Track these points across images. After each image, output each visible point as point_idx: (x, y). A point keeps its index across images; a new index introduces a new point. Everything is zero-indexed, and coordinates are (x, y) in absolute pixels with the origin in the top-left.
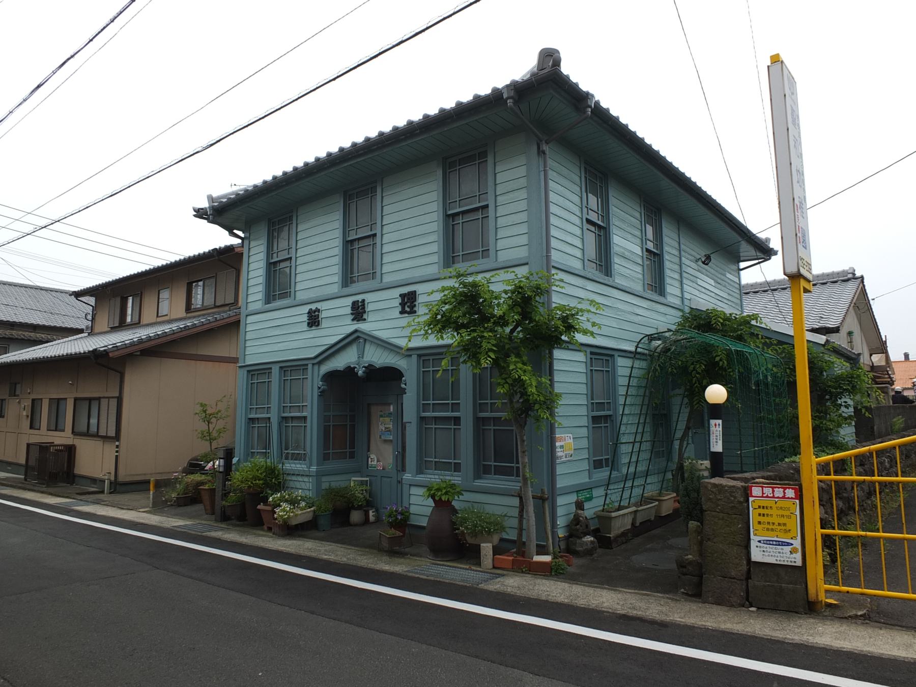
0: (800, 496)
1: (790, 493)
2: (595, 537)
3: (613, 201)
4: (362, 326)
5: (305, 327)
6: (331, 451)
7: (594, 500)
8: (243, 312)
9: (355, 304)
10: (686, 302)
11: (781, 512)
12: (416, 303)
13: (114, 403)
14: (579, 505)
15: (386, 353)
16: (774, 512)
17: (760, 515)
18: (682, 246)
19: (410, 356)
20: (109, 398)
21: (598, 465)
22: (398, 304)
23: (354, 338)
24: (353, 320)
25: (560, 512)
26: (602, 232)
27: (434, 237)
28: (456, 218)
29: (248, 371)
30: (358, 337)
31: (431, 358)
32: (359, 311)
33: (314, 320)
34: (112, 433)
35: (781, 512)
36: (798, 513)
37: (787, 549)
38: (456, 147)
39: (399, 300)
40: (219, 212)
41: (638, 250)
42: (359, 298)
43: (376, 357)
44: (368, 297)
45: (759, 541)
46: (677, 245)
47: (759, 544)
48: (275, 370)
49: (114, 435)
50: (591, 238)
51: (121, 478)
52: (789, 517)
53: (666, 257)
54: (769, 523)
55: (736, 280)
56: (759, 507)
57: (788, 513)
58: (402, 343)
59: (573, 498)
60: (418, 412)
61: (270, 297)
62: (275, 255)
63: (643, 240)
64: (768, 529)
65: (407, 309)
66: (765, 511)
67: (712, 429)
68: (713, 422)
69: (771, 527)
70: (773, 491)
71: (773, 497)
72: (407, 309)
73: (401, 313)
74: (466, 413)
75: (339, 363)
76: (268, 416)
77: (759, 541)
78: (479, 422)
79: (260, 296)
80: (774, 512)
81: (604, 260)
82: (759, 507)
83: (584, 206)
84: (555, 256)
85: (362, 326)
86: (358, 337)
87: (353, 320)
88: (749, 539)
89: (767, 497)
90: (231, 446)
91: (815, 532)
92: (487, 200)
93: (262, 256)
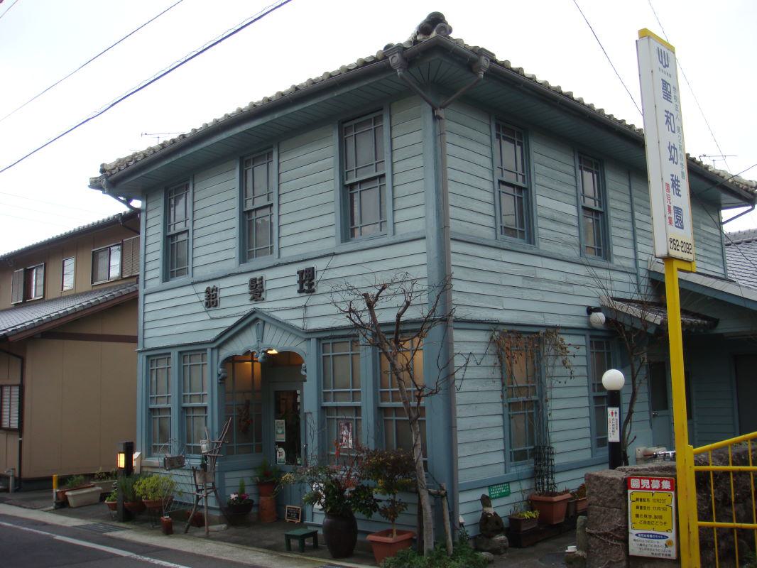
0: (674, 487)
1: (666, 484)
2: (506, 535)
3: (535, 157)
4: (259, 306)
5: (201, 307)
6: (235, 445)
7: (511, 495)
8: (141, 292)
9: (253, 281)
10: (641, 264)
11: (657, 505)
12: (315, 281)
13: (16, 391)
14: (485, 501)
15: (286, 336)
16: (651, 504)
17: (637, 507)
18: (635, 199)
19: (310, 339)
20: (11, 386)
21: (518, 457)
22: (295, 282)
23: (251, 321)
24: (251, 299)
25: (462, 509)
26: (523, 195)
27: (331, 208)
28: (355, 187)
29: (148, 357)
30: (257, 319)
31: (331, 341)
32: (257, 290)
33: (212, 300)
34: (15, 425)
35: (657, 505)
36: (673, 505)
37: (663, 542)
38: (349, 106)
39: (297, 278)
40: (114, 180)
41: (572, 210)
42: (257, 275)
43: (275, 343)
44: (268, 275)
45: (637, 535)
46: (627, 199)
47: (637, 538)
48: (175, 354)
49: (17, 427)
50: (509, 204)
51: (26, 475)
52: (665, 509)
53: (612, 214)
54: (646, 516)
55: (716, 232)
56: (637, 499)
57: (663, 505)
58: (299, 324)
59: (477, 495)
60: (319, 401)
61: (168, 274)
62: (172, 227)
63: (580, 195)
64: (645, 522)
65: (306, 288)
66: (642, 504)
67: (610, 417)
68: (610, 410)
69: (647, 520)
70: (651, 483)
71: (651, 489)
72: (306, 288)
73: (300, 292)
74: (367, 403)
75: (237, 347)
76: (168, 406)
77: (637, 535)
78: (381, 411)
79: (158, 273)
80: (651, 504)
81: (522, 228)
82: (637, 499)
83: (497, 164)
84: (454, 226)
85: (259, 306)
86: (257, 319)
87: (251, 299)
88: (628, 533)
89: (645, 489)
90: (132, 443)
91: (692, 523)
92: (383, 168)
93: (160, 229)
